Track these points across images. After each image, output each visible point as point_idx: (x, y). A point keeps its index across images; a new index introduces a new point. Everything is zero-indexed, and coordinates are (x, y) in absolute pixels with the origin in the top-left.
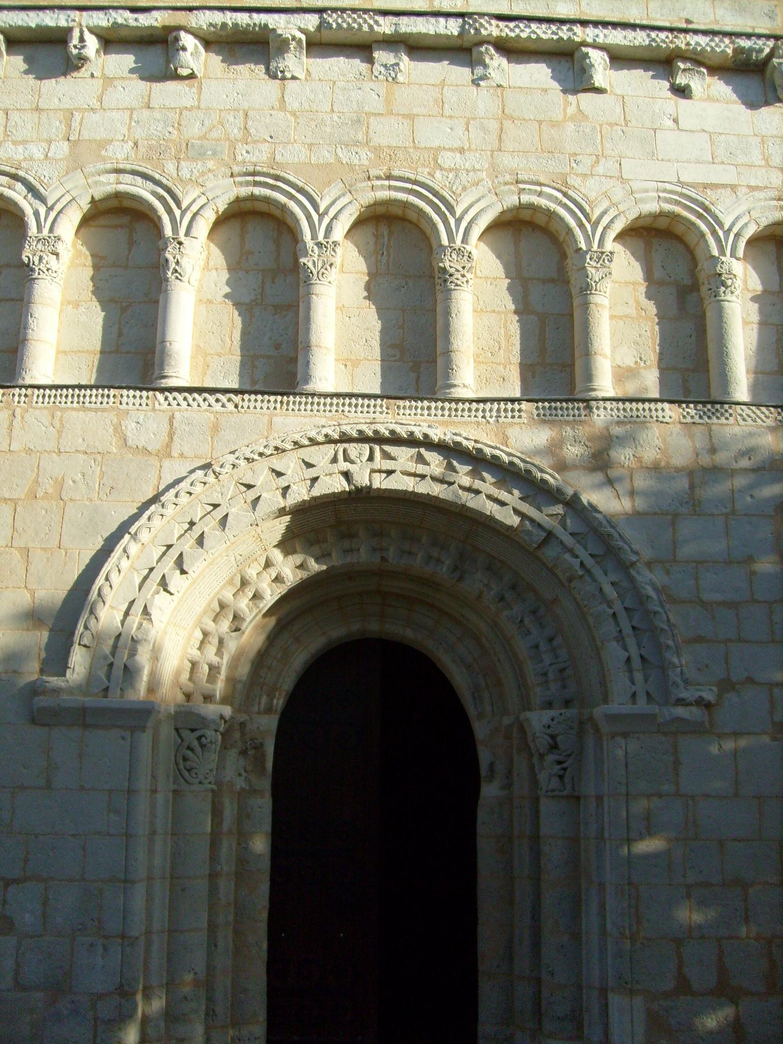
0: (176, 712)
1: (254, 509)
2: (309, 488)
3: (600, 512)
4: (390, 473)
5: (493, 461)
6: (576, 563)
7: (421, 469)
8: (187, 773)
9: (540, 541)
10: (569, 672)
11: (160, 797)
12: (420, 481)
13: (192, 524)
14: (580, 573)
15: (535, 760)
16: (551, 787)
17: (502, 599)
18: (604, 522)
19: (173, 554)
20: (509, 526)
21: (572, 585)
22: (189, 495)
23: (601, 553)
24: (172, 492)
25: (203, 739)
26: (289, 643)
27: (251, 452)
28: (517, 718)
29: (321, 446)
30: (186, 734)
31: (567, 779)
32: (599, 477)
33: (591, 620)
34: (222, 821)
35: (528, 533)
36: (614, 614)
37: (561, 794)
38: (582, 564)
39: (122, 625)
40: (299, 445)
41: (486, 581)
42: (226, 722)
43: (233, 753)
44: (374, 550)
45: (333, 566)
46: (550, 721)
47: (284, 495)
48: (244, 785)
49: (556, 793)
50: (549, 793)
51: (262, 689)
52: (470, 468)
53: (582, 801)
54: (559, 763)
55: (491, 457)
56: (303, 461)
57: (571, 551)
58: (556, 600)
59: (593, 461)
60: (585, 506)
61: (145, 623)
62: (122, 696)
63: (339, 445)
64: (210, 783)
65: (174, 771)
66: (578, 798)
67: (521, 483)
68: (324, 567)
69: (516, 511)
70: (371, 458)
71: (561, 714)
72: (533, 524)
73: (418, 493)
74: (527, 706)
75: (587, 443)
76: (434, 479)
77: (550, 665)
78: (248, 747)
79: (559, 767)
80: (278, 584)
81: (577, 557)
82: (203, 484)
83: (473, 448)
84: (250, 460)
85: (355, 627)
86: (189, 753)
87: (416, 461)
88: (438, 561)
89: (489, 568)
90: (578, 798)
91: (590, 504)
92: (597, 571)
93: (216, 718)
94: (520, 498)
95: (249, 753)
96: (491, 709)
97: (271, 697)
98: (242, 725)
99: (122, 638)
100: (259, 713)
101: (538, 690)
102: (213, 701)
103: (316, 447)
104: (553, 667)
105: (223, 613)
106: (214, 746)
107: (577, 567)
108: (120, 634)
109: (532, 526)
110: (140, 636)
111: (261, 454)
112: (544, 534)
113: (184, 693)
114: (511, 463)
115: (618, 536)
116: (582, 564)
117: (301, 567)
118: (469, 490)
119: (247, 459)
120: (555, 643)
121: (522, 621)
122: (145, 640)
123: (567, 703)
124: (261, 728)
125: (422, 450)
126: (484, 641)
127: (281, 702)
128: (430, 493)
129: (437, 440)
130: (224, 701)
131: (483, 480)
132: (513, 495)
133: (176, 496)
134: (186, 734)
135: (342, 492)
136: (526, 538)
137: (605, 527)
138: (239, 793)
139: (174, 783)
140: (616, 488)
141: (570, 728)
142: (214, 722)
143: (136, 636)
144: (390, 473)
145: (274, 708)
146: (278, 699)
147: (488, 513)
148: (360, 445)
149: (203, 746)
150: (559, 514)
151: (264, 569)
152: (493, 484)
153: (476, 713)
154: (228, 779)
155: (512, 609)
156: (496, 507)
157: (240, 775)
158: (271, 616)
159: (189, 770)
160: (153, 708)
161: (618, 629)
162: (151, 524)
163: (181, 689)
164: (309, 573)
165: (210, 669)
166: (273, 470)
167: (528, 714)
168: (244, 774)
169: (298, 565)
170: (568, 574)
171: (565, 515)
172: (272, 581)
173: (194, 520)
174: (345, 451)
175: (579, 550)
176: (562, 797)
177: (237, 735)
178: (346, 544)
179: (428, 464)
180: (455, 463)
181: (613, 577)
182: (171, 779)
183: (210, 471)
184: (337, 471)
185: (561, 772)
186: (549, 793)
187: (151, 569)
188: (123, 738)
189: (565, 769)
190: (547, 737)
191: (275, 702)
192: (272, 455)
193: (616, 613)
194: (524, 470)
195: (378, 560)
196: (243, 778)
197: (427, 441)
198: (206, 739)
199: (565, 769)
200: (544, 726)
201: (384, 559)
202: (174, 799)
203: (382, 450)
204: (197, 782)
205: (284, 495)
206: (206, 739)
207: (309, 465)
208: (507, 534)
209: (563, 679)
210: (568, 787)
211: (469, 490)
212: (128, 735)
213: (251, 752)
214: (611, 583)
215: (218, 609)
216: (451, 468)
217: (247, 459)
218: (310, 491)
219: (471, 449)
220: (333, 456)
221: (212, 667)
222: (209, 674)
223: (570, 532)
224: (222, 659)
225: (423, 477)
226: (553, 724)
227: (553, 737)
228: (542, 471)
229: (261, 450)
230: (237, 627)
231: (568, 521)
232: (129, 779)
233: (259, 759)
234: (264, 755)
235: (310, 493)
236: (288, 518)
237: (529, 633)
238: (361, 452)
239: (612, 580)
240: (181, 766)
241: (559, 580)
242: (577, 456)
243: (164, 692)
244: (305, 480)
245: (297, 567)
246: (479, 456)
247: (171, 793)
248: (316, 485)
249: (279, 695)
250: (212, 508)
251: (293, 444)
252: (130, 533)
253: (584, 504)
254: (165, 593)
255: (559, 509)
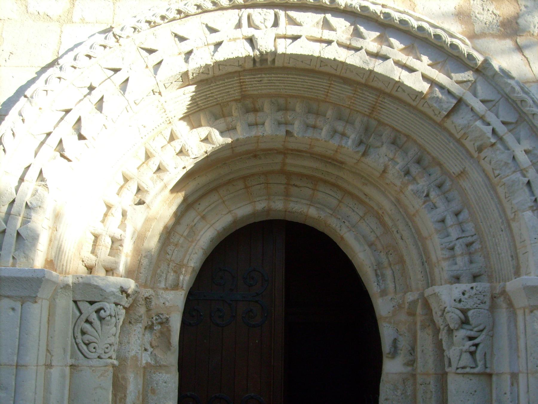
0: (74, 283)
1: (156, 73)
2: (212, 53)
3: (512, 78)
4: (295, 38)
5: (402, 27)
6: (488, 130)
7: (327, 35)
8: (85, 347)
9: (450, 109)
10: (476, 246)
11: (55, 372)
12: (326, 46)
13: (91, 88)
14: (493, 140)
15: (443, 335)
16: (462, 364)
17: (407, 173)
18: (517, 88)
19: (72, 118)
20: (418, 92)
21: (483, 155)
22: (88, 58)
23: (513, 120)
24: (72, 55)
25: (102, 311)
26: (196, 221)
27: (153, 16)
28: (422, 294)
29: (225, 12)
30: (84, 306)
31: (479, 356)
32: (508, 43)
33: (501, 191)
34: (125, 396)
35: (438, 100)
36: (529, 183)
37: (473, 371)
38: (494, 131)
39: (17, 191)
40: (202, 9)
41: (391, 156)
42: (128, 296)
43: (138, 328)
44: (279, 123)
45: (238, 140)
46: (461, 295)
47: (187, 60)
48: (149, 361)
49: (468, 370)
50: (459, 371)
51: (169, 265)
52: (378, 34)
53: (494, 378)
54: (471, 338)
55: (399, 21)
56: (207, 26)
57: (482, 118)
58: (463, 173)
59: (502, 29)
60: (497, 72)
61: (41, 190)
62: (14, 265)
63: (243, 10)
64: (110, 358)
65: (72, 346)
66: (490, 375)
67: (429, 50)
68: (229, 140)
69: (425, 78)
70: (276, 24)
71: (472, 288)
72: (443, 91)
73: (324, 58)
74: (430, 282)
75: (495, 11)
76: (340, 45)
77: (457, 239)
78: (154, 322)
79: (471, 343)
80: (182, 157)
81: (489, 124)
82: (103, 48)
83: (381, 12)
84: (152, 24)
85: (260, 206)
86: (88, 326)
87: (322, 27)
88: (343, 135)
89: (394, 143)
90: (490, 375)
91: (502, 70)
92: (510, 139)
93: (117, 291)
94: (429, 65)
95: (155, 328)
96: (393, 286)
97: (177, 273)
98: (147, 300)
99: (15, 205)
100: (166, 289)
101: (445, 264)
102: (115, 274)
103: (220, 12)
104: (461, 240)
105: (127, 185)
106: (114, 319)
107: (490, 134)
108: (14, 201)
109: (442, 94)
110: (34, 203)
111: (163, 18)
112: (454, 102)
113: (85, 266)
114: (420, 28)
115: (531, 102)
116: (494, 131)
117: (206, 140)
118: (376, 56)
119: (149, 22)
120: (461, 217)
121: (427, 195)
122: (40, 207)
123: (475, 278)
124: (167, 304)
125: (329, 16)
126: (386, 219)
127: (187, 278)
128: (337, 58)
129: (343, 5)
130: (130, 273)
131: (391, 46)
132: (421, 61)
133: (75, 59)
134: (84, 306)
135: (246, 56)
136: (435, 105)
137: (518, 93)
138: (144, 368)
139: (71, 357)
140: (527, 56)
141: (482, 303)
142: (114, 294)
143: (31, 203)
144: (295, 38)
145: (180, 285)
146: (185, 276)
147: (397, 79)
148: (265, 10)
149: (101, 319)
150: (469, 81)
151: (169, 143)
152: (402, 50)
153: (379, 290)
154: (133, 353)
155: (418, 183)
156: (405, 73)
157: (146, 350)
158: (177, 192)
159: (87, 345)
160: (44, 277)
161: (533, 198)
162: (48, 87)
163: (83, 261)
164: (214, 146)
165: (113, 242)
166: (176, 35)
167: (437, 289)
168: (150, 350)
169: (203, 138)
170: (478, 144)
171: (475, 82)
172: (177, 154)
173: (94, 85)
174: (249, 17)
175: (491, 117)
176: (473, 374)
177: (142, 310)
178: (251, 118)
179: (334, 30)
180: (362, 29)
181: (527, 145)
182: (69, 353)
183: (111, 34)
184: (241, 37)
185: (473, 348)
186: (459, 371)
187: (49, 134)
188: (13, 309)
189: (476, 345)
190: (458, 312)
191: (181, 277)
192: (174, 19)
193: (531, 181)
194: (434, 35)
195: (282, 132)
196: (149, 353)
197: (334, 6)
198: (105, 311)
199: (476, 345)
200: (455, 300)
201: (288, 133)
202: (71, 373)
203: (288, 17)
204: (96, 357)
205: (187, 60)
206: (105, 311)
207: (212, 30)
208: (414, 104)
209: (470, 253)
210: (480, 364)
211: (376, 56)
212: (18, 305)
213: (157, 327)
214: (525, 151)
215: (122, 182)
216: (357, 34)
217: (149, 22)
218: (213, 55)
219: (379, 14)
220: (237, 22)
221: (114, 240)
222: (112, 247)
223: (481, 99)
224: (125, 231)
225: (329, 42)
226: (463, 298)
227: (464, 312)
228: (452, 36)
229: (164, 13)
230: (140, 200)
231: (479, 88)
232: (18, 353)
233: (165, 335)
234: (169, 330)
235: (213, 58)
236: (193, 88)
237: (435, 207)
238: (266, 18)
239: (526, 148)
240: (79, 340)
241: (468, 151)
242: (486, 24)
243: (65, 264)
244: (208, 44)
245: (202, 141)
246: (386, 22)
247: (68, 368)
248: (219, 49)
249: (186, 271)
250: (113, 73)
251: (196, 7)
252: (25, 96)
253: (495, 70)
254: (62, 158)
255: (468, 76)
